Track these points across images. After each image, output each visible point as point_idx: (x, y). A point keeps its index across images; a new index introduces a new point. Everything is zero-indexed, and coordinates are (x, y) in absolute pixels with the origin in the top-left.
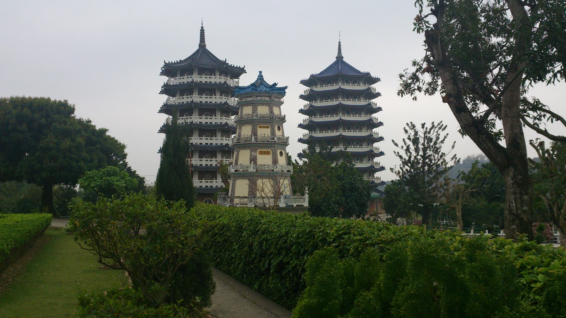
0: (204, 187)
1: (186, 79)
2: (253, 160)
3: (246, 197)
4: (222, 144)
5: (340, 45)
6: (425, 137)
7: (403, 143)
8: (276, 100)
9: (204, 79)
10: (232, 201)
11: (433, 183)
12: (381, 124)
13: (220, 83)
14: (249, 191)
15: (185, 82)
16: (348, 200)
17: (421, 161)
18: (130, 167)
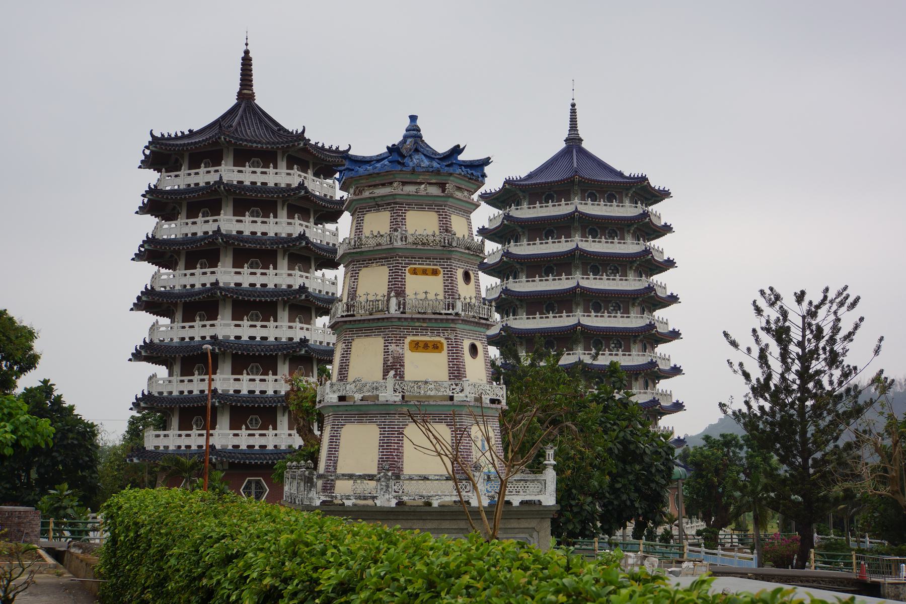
0: (243, 447)
1: (203, 177)
3: (371, 477)
4: (291, 339)
5: (573, 112)
6: (806, 326)
7: (753, 339)
8: (459, 194)
9: (249, 176)
10: (328, 487)
12: (673, 299)
13: (289, 185)
14: (381, 460)
15: (202, 184)
16: (618, 486)
17: (795, 387)
18: (60, 397)
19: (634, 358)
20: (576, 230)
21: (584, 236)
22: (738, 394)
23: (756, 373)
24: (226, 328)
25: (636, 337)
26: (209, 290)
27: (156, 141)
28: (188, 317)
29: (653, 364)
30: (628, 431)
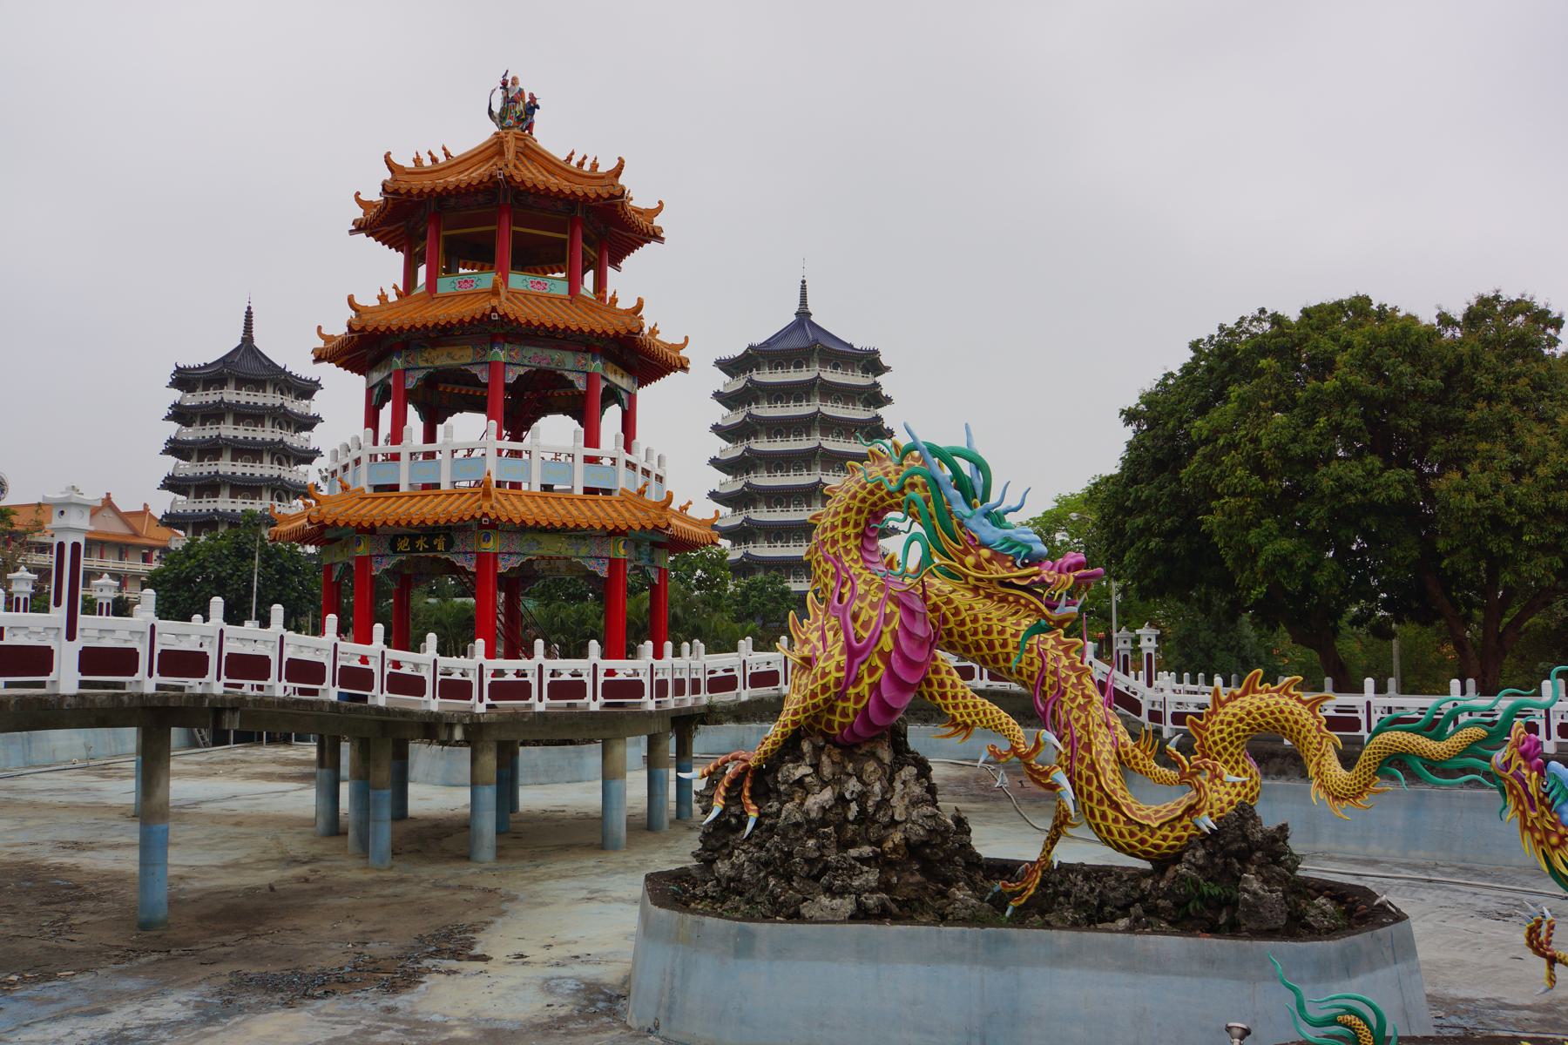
1: (211, 397)
5: (804, 288)
27: (179, 370)
28: (198, 496)
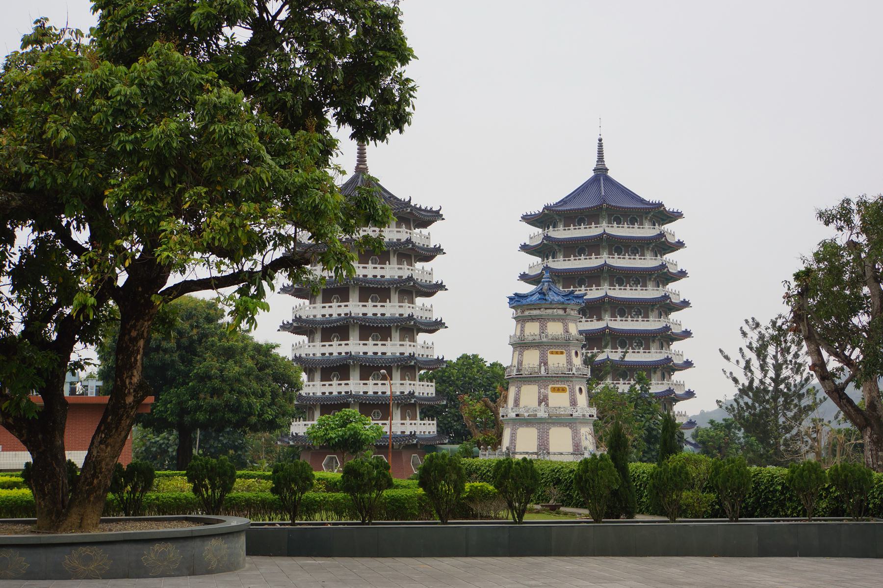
2: (543, 400)
5: (600, 146)
11: (792, 428)
17: (771, 388)
19: (654, 355)
20: (604, 248)
21: (610, 253)
22: (730, 392)
23: (744, 381)
24: (355, 346)
25: (653, 305)
26: (344, 319)
29: (669, 360)
30: (652, 421)
